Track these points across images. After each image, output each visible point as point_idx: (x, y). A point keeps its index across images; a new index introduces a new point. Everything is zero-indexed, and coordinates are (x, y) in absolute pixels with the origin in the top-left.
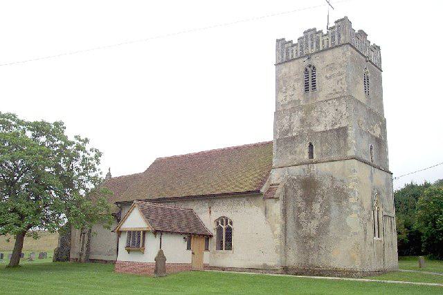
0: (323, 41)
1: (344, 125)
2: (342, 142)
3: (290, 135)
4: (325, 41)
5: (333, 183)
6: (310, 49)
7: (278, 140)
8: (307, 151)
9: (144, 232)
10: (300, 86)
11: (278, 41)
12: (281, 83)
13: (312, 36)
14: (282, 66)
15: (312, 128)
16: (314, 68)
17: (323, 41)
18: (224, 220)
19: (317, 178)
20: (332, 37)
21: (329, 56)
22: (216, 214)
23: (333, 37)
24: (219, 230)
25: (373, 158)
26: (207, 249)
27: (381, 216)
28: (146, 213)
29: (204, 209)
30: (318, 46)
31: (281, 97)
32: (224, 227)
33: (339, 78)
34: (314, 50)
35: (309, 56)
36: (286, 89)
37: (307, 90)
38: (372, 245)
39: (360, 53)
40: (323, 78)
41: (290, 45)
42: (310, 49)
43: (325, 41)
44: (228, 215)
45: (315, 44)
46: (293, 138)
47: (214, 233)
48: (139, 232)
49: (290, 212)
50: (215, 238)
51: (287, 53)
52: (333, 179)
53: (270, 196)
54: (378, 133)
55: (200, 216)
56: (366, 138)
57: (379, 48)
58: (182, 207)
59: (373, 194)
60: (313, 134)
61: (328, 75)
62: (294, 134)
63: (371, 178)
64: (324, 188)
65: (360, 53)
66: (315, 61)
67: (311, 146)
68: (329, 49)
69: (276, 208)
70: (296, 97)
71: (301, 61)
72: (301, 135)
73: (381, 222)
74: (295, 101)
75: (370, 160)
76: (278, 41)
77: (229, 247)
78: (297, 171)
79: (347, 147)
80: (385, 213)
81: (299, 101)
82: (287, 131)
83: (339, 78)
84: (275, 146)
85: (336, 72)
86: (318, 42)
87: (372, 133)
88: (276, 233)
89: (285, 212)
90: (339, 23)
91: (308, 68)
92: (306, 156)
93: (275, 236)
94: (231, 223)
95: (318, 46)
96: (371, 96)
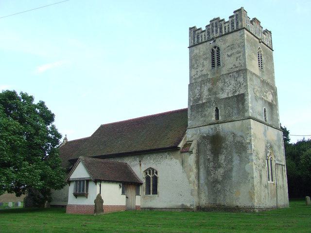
0: (225, 27)
1: (242, 92)
2: (240, 106)
3: (200, 102)
4: (227, 28)
5: (234, 139)
6: (215, 33)
7: (191, 106)
8: (214, 114)
9: (88, 181)
10: (208, 64)
11: (190, 29)
12: (194, 62)
13: (216, 23)
14: (193, 48)
15: (217, 96)
16: (218, 48)
17: (225, 27)
18: (150, 170)
19: (222, 134)
20: (232, 23)
21: (229, 38)
22: (144, 167)
23: (233, 23)
24: (148, 179)
25: (267, 119)
26: (138, 194)
27: (274, 164)
28: (88, 167)
29: (136, 162)
30: (221, 32)
31: (194, 72)
32: (151, 176)
33: (238, 55)
34: (218, 35)
35: (214, 39)
36: (198, 66)
37: (213, 65)
38: (266, 187)
39: (255, 36)
40: (226, 56)
41: (200, 31)
42: (215, 33)
43: (227, 28)
44: (154, 167)
46: (203, 104)
47: (144, 181)
48: (84, 181)
49: (202, 161)
50: (144, 185)
51: (198, 38)
52: (234, 135)
53: (186, 149)
54: (270, 98)
55: (132, 168)
56: (260, 102)
58: (119, 160)
59: (266, 146)
60: (218, 100)
62: (204, 101)
63: (265, 134)
64: (227, 142)
65: (255, 36)
66: (219, 43)
67: (217, 110)
68: (229, 33)
69: (191, 159)
70: (205, 72)
71: (208, 43)
72: (209, 101)
73: (274, 169)
74: (204, 75)
75: (263, 120)
76: (190, 29)
77: (155, 192)
78: (206, 130)
80: (277, 162)
81: (207, 74)
82: (199, 99)
83: (238, 55)
84: (189, 112)
85: (234, 51)
86: (221, 29)
87: (265, 98)
88: (191, 179)
89: (197, 162)
91: (214, 49)
92: (214, 118)
93: (190, 182)
94: (157, 173)
95: (221, 32)
96: (264, 69)
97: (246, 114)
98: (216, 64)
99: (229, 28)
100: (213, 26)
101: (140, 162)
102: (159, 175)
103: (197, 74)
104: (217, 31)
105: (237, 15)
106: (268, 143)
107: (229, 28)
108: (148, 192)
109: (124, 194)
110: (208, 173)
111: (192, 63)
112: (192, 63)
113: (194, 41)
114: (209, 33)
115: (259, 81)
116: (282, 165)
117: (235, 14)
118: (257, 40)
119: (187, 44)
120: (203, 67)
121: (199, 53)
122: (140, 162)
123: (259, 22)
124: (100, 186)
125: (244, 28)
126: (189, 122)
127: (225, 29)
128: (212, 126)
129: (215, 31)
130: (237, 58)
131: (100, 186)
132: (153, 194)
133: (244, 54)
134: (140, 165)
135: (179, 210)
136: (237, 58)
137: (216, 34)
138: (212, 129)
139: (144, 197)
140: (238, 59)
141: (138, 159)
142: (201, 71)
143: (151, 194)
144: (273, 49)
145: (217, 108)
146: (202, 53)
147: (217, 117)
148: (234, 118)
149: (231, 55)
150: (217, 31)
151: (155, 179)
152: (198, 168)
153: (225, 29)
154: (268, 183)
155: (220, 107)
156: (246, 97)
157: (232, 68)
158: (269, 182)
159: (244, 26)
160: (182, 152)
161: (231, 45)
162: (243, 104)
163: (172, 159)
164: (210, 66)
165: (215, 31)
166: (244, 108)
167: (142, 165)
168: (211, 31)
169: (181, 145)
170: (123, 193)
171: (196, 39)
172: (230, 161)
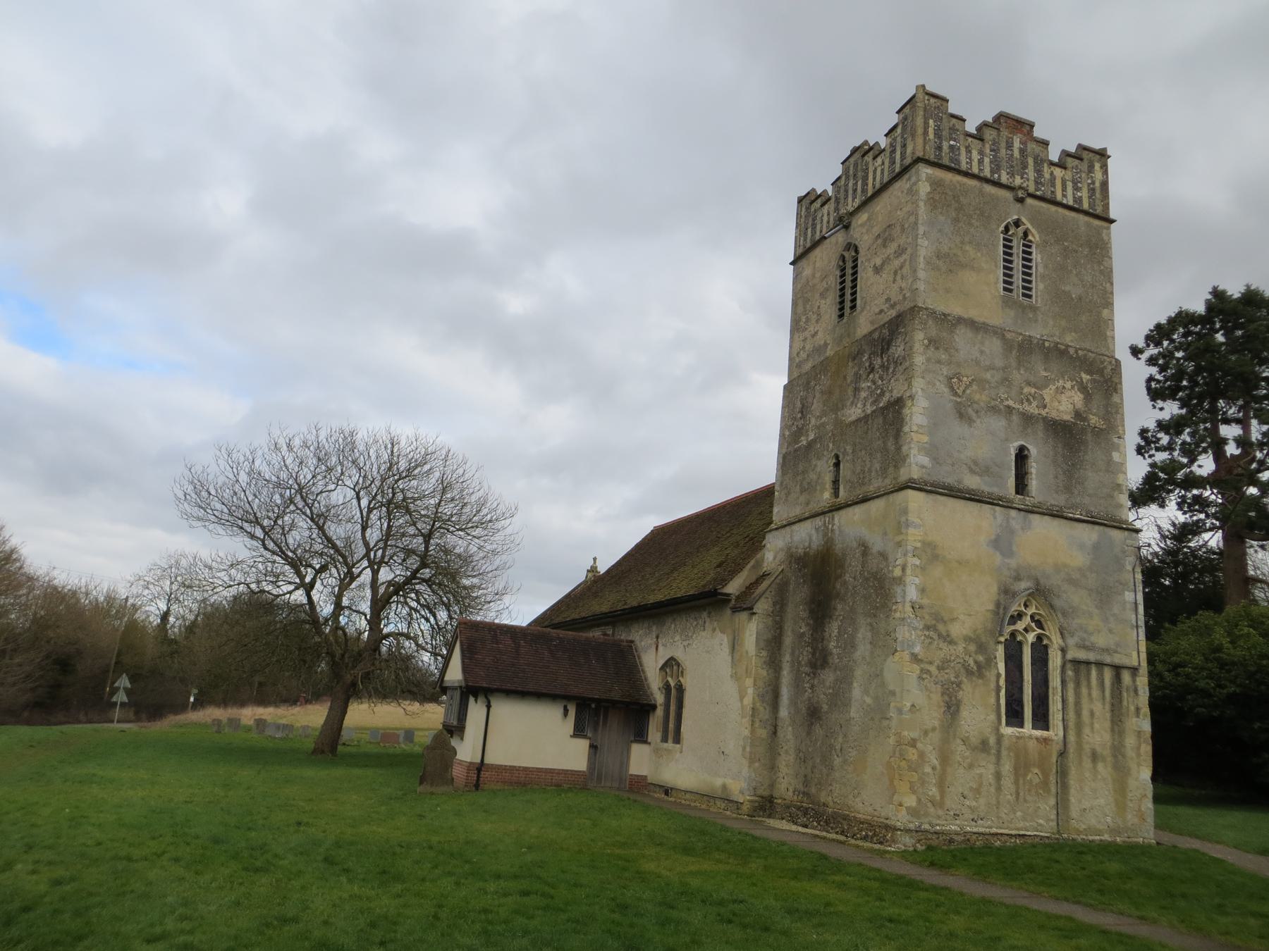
0: (875, 171)
1: (896, 394)
2: (891, 445)
12: (800, 309)
14: (804, 262)
16: (857, 251)
23: (893, 151)
26: (641, 737)
27: (1055, 660)
30: (864, 191)
42: (850, 199)
45: (860, 183)
47: (659, 698)
50: (660, 712)
52: (865, 549)
53: (744, 604)
57: (1102, 155)
59: (1007, 592)
61: (878, 261)
69: (752, 631)
73: (1055, 681)
77: (677, 740)
79: (897, 459)
83: (897, 263)
90: (907, 110)
91: (846, 254)
92: (827, 495)
97: (902, 471)
98: (847, 311)
99: (883, 170)
100: (847, 178)
101: (657, 637)
102: (687, 681)
103: (804, 347)
104: (855, 191)
105: (905, 119)
106: (1018, 578)
107: (883, 170)
108: (665, 739)
109: (585, 737)
110: (797, 684)
111: (796, 314)
112: (796, 314)
113: (805, 240)
114: (837, 201)
115: (994, 345)
116: (1117, 669)
117: (902, 116)
118: (1008, 195)
119: (787, 247)
120: (817, 321)
121: (813, 276)
122: (657, 637)
123: (1023, 126)
124: (489, 707)
125: (919, 160)
126: (775, 510)
127: (874, 179)
128: (818, 521)
129: (850, 192)
130: (896, 273)
131: (489, 707)
132: (1034, 727)
133: (914, 257)
134: (657, 649)
135: (719, 803)
136: (896, 273)
137: (853, 201)
138: (817, 530)
139: (657, 751)
140: (898, 277)
141: (654, 628)
142: (813, 336)
143: (670, 740)
144: (1112, 216)
145: (837, 457)
146: (818, 275)
147: (1021, 487)
148: (871, 489)
149: (883, 264)
150: (855, 191)
151: (680, 689)
152: (773, 663)
153: (874, 179)
154: (1000, 738)
155: (845, 453)
156: (906, 411)
157: (881, 311)
158: (1008, 731)
159: (920, 154)
160: (735, 610)
161: (885, 231)
162: (898, 435)
163: (714, 630)
164: (835, 316)
165: (850, 192)
166: (899, 449)
167: (661, 648)
168: (842, 195)
169: (733, 587)
170: (579, 732)
171: (809, 230)
172: (850, 645)
